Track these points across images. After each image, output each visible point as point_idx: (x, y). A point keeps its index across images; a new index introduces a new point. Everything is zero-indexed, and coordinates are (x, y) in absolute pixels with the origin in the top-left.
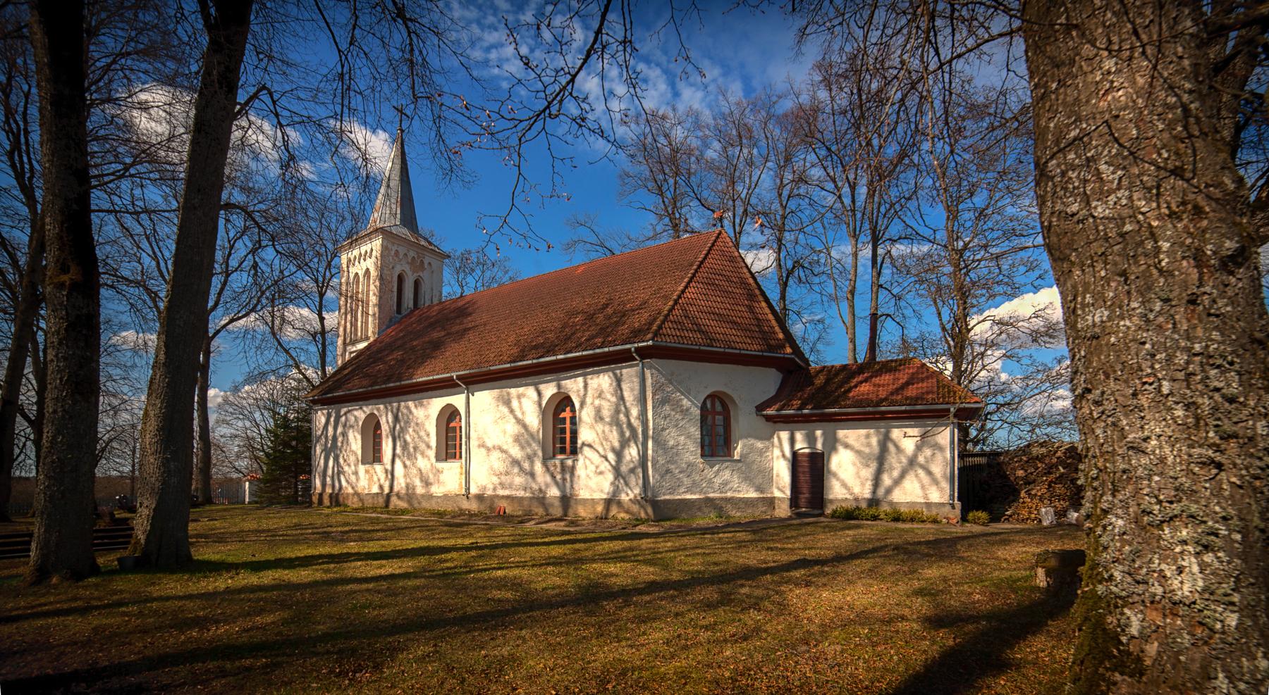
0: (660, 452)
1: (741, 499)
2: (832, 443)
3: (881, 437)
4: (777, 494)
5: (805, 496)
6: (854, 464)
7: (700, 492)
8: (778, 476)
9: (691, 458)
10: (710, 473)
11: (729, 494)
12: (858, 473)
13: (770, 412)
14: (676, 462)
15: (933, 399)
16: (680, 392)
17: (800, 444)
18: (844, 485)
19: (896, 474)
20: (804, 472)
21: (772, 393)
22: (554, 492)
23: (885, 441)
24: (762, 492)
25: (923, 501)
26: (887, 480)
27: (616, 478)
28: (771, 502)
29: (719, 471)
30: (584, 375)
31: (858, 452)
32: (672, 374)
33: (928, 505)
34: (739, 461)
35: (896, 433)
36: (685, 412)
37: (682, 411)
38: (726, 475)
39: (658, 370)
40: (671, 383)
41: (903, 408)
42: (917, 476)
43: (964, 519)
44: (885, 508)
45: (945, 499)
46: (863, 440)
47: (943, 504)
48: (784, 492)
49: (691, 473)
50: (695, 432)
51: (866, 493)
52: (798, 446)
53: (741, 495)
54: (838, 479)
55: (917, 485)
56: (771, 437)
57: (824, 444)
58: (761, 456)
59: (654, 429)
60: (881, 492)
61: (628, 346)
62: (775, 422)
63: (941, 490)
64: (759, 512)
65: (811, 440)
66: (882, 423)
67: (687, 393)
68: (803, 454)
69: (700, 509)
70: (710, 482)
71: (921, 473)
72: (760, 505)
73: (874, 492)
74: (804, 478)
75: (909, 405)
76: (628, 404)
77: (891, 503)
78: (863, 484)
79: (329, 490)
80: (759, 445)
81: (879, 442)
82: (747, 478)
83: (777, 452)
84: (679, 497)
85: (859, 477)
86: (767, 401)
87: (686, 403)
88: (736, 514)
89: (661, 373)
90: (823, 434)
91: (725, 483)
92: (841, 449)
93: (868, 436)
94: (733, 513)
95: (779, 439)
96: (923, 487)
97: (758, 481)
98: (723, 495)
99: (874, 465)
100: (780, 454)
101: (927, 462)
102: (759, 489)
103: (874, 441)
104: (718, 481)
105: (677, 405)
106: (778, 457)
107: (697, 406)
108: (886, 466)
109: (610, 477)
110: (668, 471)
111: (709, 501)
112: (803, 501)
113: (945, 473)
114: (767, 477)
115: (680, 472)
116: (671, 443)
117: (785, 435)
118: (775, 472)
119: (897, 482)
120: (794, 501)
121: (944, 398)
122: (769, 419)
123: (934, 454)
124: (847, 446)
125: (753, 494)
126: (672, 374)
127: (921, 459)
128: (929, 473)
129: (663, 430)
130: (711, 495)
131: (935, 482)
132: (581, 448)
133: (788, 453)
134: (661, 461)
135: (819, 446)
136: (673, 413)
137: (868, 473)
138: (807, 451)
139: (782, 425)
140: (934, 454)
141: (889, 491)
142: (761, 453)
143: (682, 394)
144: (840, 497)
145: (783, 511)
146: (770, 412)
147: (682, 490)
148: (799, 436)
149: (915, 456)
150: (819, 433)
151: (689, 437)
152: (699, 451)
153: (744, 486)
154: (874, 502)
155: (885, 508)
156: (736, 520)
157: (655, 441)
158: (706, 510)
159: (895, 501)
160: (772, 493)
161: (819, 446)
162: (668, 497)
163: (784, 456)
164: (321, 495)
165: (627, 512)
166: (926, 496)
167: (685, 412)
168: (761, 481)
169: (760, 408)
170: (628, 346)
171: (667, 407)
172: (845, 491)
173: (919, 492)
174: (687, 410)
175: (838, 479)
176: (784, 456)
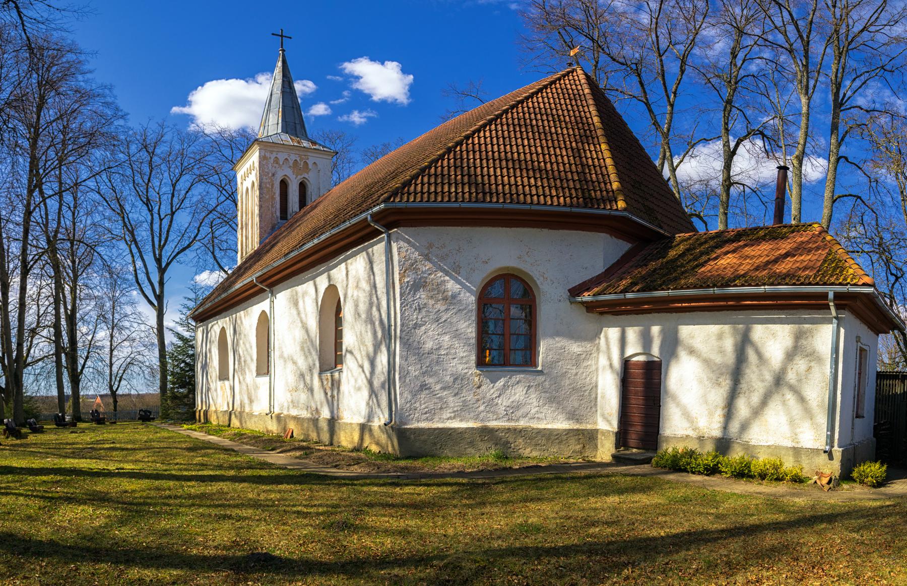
0: (412, 359)
1: (539, 432)
2: (672, 345)
3: (739, 338)
4: (602, 425)
5: (636, 429)
6: (700, 381)
7: (476, 418)
8: (603, 397)
9: (460, 367)
10: (490, 390)
11: (522, 424)
12: (704, 396)
13: (587, 297)
14: (436, 374)
15: (808, 277)
16: (443, 271)
17: (633, 348)
18: (687, 415)
19: (756, 399)
20: (636, 393)
21: (599, 269)
22: (325, 414)
23: (744, 343)
24: (578, 421)
25: (790, 444)
26: (743, 408)
27: (370, 396)
28: (590, 437)
29: (505, 387)
30: (365, 249)
31: (707, 362)
32: (431, 246)
33: (797, 451)
34: (541, 372)
35: (759, 332)
36: (451, 300)
37: (445, 299)
38: (518, 393)
39: (409, 242)
40: (429, 260)
41: (762, 289)
42: (784, 403)
43: (846, 476)
44: (736, 455)
45: (821, 443)
46: (714, 342)
47: (815, 451)
48: (610, 424)
49: (461, 389)
50: (469, 329)
51: (715, 431)
52: (629, 352)
53: (542, 425)
54: (678, 405)
55: (783, 419)
56: (597, 335)
57: (662, 348)
58: (577, 365)
59: (402, 325)
60: (734, 427)
61: (363, 216)
62: (602, 313)
63: (816, 426)
64: (567, 454)
65: (646, 340)
66: (741, 315)
67: (455, 271)
68: (637, 364)
69: (472, 444)
70: (491, 403)
71: (790, 396)
72: (572, 441)
73: (725, 428)
74: (637, 401)
75: (772, 284)
76: (379, 293)
77: (747, 447)
78: (711, 414)
79: (204, 408)
80: (575, 348)
81: (736, 345)
82: (554, 398)
83: (603, 361)
84: (440, 425)
85: (706, 402)
86: (590, 281)
87: (452, 286)
88: (531, 454)
89: (413, 246)
90: (662, 332)
91: (517, 407)
92: (683, 354)
93: (720, 337)
94: (526, 452)
95: (607, 338)
96: (792, 422)
97: (573, 403)
98: (512, 424)
99: (726, 383)
100: (607, 363)
101: (800, 381)
102: (572, 416)
103: (729, 344)
104: (503, 403)
105: (438, 290)
106: (604, 368)
107: (470, 291)
108: (743, 385)
109: (365, 393)
110: (424, 387)
111: (487, 433)
112: (633, 439)
113: (823, 401)
114: (589, 397)
115: (444, 388)
116: (429, 345)
117: (613, 333)
118: (599, 391)
119: (757, 411)
120: (622, 438)
121: (824, 276)
122: (590, 307)
123: (809, 369)
124: (692, 351)
125: (562, 424)
126: (431, 246)
127: (791, 377)
128: (802, 399)
129: (416, 326)
130: (493, 424)
131: (808, 413)
132: (346, 354)
133: (617, 363)
134: (414, 371)
135: (656, 351)
136: (431, 302)
137: (718, 396)
138: (641, 358)
139: (610, 317)
140: (810, 368)
141: (744, 427)
142: (578, 360)
143: (447, 274)
144: (681, 432)
145: (605, 451)
146: (587, 297)
147: (446, 414)
148: (632, 334)
149: (783, 371)
150: (655, 330)
151: (457, 335)
152: (473, 358)
153: (548, 410)
154: (723, 445)
155: (736, 455)
156: (532, 463)
157: (407, 344)
158: (482, 446)
159: (753, 443)
160: (595, 423)
161: (656, 351)
162: (423, 425)
163: (611, 366)
164: (200, 411)
165: (378, 444)
166: (795, 437)
167: (451, 300)
168: (576, 404)
169: (575, 292)
170: (363, 216)
171: (422, 295)
172: (686, 424)
173: (785, 429)
174: (454, 296)
175: (678, 405)
176: (611, 366)
